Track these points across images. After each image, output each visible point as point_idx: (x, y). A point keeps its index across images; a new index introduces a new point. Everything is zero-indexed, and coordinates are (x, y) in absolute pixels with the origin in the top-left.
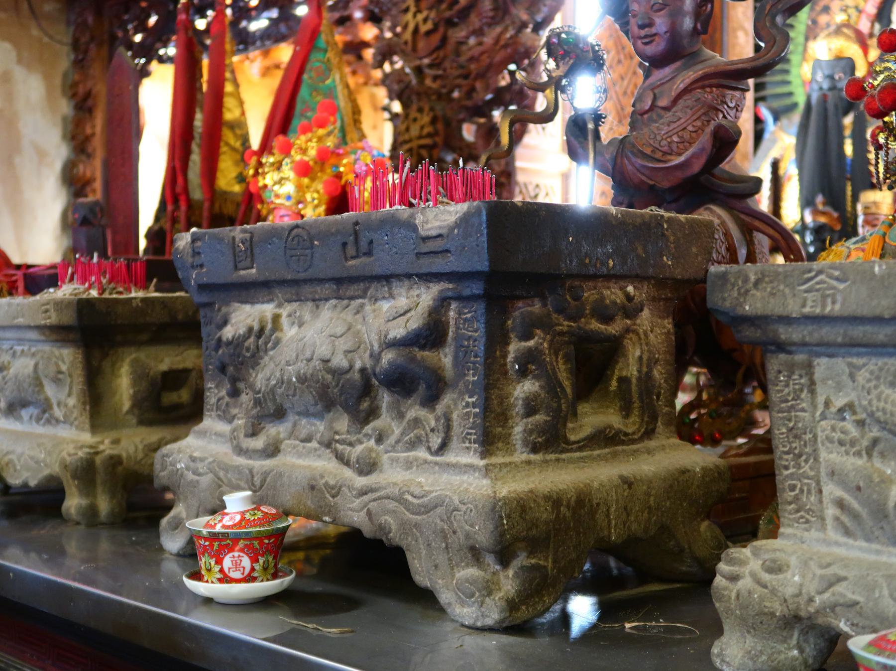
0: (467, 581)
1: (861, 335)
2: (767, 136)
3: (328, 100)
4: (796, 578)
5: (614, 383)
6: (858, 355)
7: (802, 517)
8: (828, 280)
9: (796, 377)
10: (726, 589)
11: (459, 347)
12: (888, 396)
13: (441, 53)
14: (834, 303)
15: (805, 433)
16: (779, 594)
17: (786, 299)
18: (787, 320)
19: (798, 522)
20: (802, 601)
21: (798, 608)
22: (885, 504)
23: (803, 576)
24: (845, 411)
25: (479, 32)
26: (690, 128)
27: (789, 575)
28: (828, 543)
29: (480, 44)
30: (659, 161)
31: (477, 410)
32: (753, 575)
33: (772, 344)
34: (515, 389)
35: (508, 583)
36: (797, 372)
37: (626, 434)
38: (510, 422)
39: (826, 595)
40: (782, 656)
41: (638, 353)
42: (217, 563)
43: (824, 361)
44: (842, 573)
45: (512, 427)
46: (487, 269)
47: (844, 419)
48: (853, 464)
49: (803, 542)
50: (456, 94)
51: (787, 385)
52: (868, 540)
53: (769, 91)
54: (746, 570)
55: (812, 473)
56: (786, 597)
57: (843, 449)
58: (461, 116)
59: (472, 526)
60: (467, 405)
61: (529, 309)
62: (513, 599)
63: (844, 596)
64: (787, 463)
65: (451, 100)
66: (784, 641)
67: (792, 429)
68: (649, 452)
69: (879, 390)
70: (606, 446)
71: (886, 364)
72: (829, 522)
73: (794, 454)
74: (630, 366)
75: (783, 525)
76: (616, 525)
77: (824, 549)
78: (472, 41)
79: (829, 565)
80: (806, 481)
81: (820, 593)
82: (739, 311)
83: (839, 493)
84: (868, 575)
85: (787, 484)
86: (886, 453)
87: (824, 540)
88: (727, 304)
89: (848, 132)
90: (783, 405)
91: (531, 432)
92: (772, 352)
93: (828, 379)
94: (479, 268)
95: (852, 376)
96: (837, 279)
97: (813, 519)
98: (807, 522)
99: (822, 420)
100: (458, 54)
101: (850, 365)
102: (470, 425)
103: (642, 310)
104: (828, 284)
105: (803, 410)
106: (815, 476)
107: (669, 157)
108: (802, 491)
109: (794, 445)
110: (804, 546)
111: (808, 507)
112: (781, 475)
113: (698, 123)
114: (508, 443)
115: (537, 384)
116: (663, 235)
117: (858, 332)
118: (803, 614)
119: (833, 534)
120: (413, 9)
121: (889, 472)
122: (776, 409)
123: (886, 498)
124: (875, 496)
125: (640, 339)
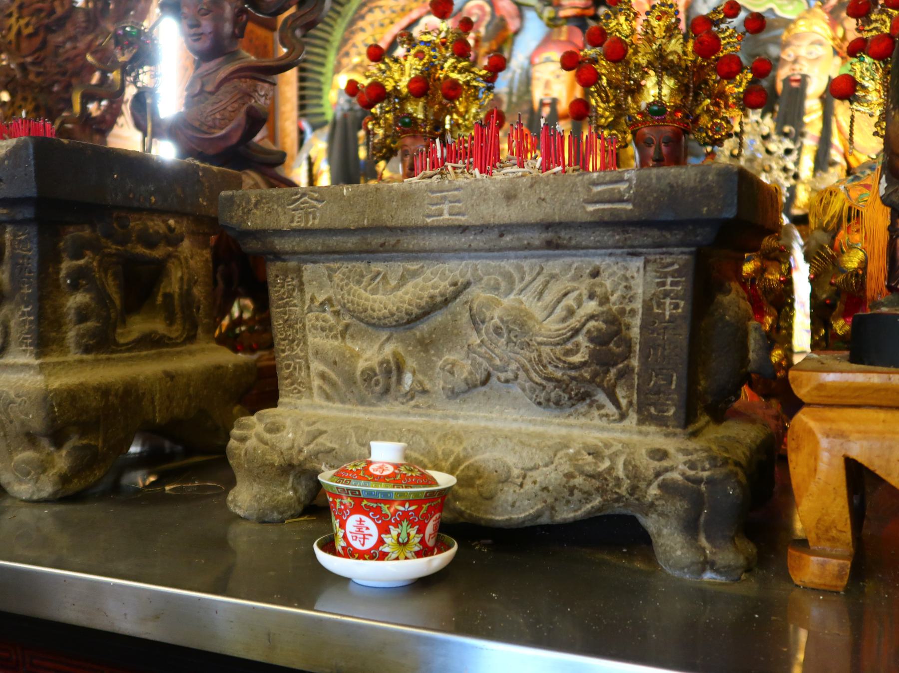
0: (23, 462)
2: (306, 142)
4: (290, 435)
5: (160, 299)
6: (334, 260)
7: (295, 389)
10: (237, 448)
11: (15, 265)
12: (356, 291)
13: (42, 54)
14: (314, 218)
18: (280, 233)
20: (294, 452)
21: (291, 458)
23: (295, 433)
25: (73, 39)
26: (230, 109)
27: (284, 433)
28: (314, 406)
29: (75, 48)
30: (206, 133)
31: (32, 318)
32: (258, 436)
33: (270, 254)
34: (68, 301)
35: (62, 461)
37: (170, 339)
38: (64, 328)
39: (312, 446)
40: (281, 497)
41: (179, 274)
42: (418, 532)
43: (310, 266)
44: (324, 428)
45: (66, 332)
46: (35, 195)
47: (324, 311)
50: (56, 88)
51: (283, 287)
52: (343, 402)
53: (309, 111)
54: (252, 432)
58: (61, 106)
59: (27, 415)
60: (23, 314)
61: (80, 233)
62: (65, 474)
63: (324, 445)
65: (51, 93)
66: (283, 484)
67: (287, 320)
68: (191, 353)
70: (152, 348)
71: (354, 267)
74: (174, 282)
76: (160, 410)
77: (310, 412)
78: (68, 45)
79: (314, 423)
81: (307, 444)
82: (244, 226)
83: (322, 367)
87: (312, 405)
88: (234, 221)
89: (361, 142)
91: (83, 336)
92: (272, 261)
94: (28, 194)
95: (330, 277)
96: (316, 200)
98: (299, 392)
100: (56, 54)
101: (329, 268)
102: (26, 331)
103: (182, 240)
105: (295, 305)
107: (213, 130)
108: (295, 368)
110: (297, 411)
113: (236, 105)
114: (62, 346)
115: (88, 296)
116: (199, 181)
117: (333, 241)
118: (295, 462)
119: (318, 400)
120: (15, 15)
123: (355, 368)
125: (181, 263)
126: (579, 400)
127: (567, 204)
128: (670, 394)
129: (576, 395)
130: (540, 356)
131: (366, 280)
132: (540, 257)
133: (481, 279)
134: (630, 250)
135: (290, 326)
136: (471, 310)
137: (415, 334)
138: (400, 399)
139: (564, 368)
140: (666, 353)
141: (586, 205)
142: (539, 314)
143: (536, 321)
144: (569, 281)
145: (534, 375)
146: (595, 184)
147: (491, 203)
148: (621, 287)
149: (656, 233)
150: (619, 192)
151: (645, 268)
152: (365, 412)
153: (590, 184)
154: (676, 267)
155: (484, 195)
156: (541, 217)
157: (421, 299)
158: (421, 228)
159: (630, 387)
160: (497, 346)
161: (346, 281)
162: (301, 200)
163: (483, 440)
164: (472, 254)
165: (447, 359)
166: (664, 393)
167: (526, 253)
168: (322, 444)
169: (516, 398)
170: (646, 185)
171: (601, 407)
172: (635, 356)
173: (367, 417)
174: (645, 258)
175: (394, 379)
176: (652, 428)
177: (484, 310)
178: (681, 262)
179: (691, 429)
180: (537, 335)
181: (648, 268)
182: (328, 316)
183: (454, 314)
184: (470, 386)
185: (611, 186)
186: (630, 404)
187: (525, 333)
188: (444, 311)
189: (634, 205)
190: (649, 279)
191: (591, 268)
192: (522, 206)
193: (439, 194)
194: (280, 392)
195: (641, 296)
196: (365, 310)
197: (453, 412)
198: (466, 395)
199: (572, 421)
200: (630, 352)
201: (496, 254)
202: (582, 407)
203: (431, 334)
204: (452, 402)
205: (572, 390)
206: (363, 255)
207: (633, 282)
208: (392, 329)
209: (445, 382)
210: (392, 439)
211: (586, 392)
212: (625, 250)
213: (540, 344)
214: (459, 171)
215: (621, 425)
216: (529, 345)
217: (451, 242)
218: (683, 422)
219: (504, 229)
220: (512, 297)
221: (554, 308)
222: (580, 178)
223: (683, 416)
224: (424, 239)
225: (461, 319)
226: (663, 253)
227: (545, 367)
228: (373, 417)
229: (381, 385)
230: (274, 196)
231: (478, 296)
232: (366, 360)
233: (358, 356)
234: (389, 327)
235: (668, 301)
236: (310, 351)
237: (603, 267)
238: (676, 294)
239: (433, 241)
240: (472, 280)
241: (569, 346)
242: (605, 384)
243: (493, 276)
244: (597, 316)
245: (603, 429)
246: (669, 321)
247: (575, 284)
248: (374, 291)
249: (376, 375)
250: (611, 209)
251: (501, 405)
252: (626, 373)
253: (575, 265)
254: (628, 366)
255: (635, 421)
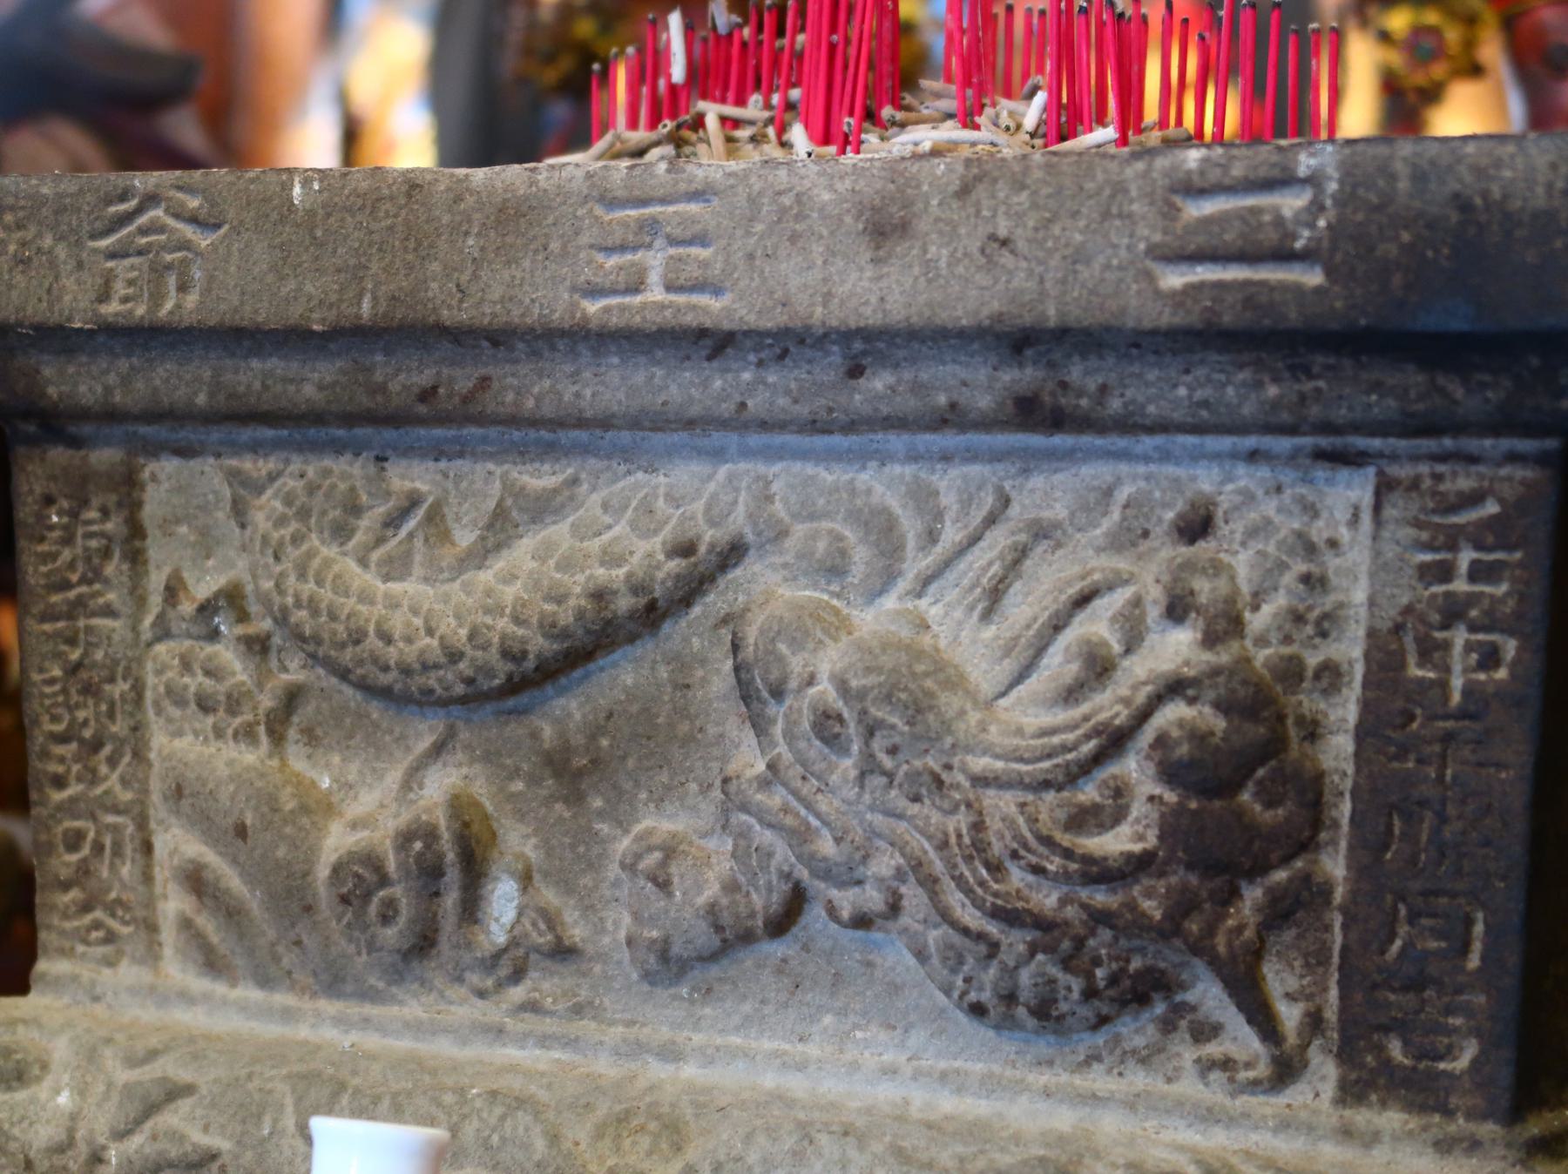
1: (257, 385)
3: (1178, 998)
4: (64, 1099)
6: (255, 448)
7: (97, 925)
8: (171, 222)
9: (93, 514)
12: (327, 563)
14: (183, 288)
15: (112, 680)
16: (13, 1146)
17: (57, 278)
18: (59, 339)
19: (87, 943)
22: (306, 874)
23: (81, 1091)
24: (216, 611)
27: (42, 1091)
28: (156, 994)
33: (27, 415)
36: (96, 502)
39: (137, 1140)
44: (184, 1075)
47: (214, 635)
48: (230, 763)
49: (96, 999)
51: (68, 540)
52: (265, 982)
55: (126, 796)
56: (32, 1154)
57: (210, 720)
63: (180, 1138)
64: (60, 769)
67: (76, 668)
69: (304, 547)
71: (327, 473)
72: (168, 935)
73: (82, 741)
75: (46, 952)
77: (148, 1014)
79: (152, 1055)
80: (111, 819)
81: (120, 1135)
84: (250, 1077)
85: (60, 829)
86: (319, 732)
87: (152, 989)
90: (55, 598)
92: (32, 441)
93: (178, 521)
95: (239, 511)
96: (194, 220)
97: (126, 930)
98: (110, 938)
99: (159, 639)
101: (234, 476)
104: (173, 231)
105: (109, 612)
106: (132, 802)
108: (98, 848)
109: (81, 715)
110: (99, 1009)
111: (113, 895)
112: (44, 802)
117: (253, 376)
119: (177, 971)
121: (326, 783)
122: (35, 610)
124: (281, 852)
126: (1123, 1003)
127: (1088, 262)
128: (1459, 991)
129: (1113, 980)
130: (978, 826)
131: (366, 524)
132: (996, 457)
133: (783, 533)
134: (1324, 442)
135: (89, 690)
136: (736, 648)
137: (535, 735)
138: (474, 978)
139: (1065, 877)
140: (1447, 833)
141: (1157, 268)
142: (984, 673)
143: (972, 695)
144: (1099, 550)
145: (955, 899)
146: (1194, 189)
147: (818, 249)
148: (1288, 579)
149: (1415, 378)
150: (1279, 221)
151: (1377, 508)
152: (340, 1021)
153: (1173, 190)
154: (1491, 508)
155: (793, 217)
156: (996, 306)
157: (560, 600)
158: (563, 333)
159: (1316, 959)
160: (825, 787)
161: (294, 526)
162: (143, 220)
163: (761, 1139)
164: (755, 440)
165: (649, 832)
166: (1439, 983)
167: (948, 440)
168: (177, 1137)
169: (895, 989)
170: (1374, 199)
171: (1205, 1032)
172: (1334, 842)
173: (347, 1040)
174: (1380, 473)
175: (451, 900)
176: (1393, 1119)
177: (782, 648)
178: (1507, 491)
179: (1534, 1128)
180: (968, 749)
181: (1390, 512)
182: (227, 654)
183: (682, 664)
184: (732, 938)
185: (1250, 201)
186: (1314, 1022)
187: (927, 740)
188: (646, 648)
189: (1329, 272)
190: (1390, 551)
191: (1180, 505)
192: (928, 265)
193: (633, 213)
194: (43, 936)
195: (1363, 612)
196: (357, 638)
197: (665, 1033)
198: (714, 971)
199: (1098, 1080)
200: (1316, 824)
201: (837, 440)
202: (1137, 1030)
203: (594, 734)
204: (662, 994)
205: (1097, 962)
206: (361, 432)
207: (1332, 562)
208: (456, 710)
209: (636, 916)
210: (397, 1114)
211: (1148, 971)
212: (1307, 441)
213: (982, 781)
214: (743, 133)
215: (1280, 1100)
216: (939, 783)
217: (674, 393)
218: (1504, 1102)
219: (863, 347)
220: (890, 602)
221: (1040, 651)
222: (1140, 166)
223: (1505, 1075)
224: (574, 377)
225: (704, 681)
226: (1443, 458)
227: (996, 868)
228: (372, 1041)
229: (402, 920)
230: (44, 201)
231: (768, 596)
232: (354, 825)
233: (328, 808)
234: (445, 703)
235: (1460, 637)
236: (156, 787)
237: (1224, 502)
238: (1489, 613)
239: (611, 385)
240: (750, 537)
241: (1089, 793)
242: (1221, 943)
243: (826, 525)
244: (1195, 682)
245: (1209, 1116)
246: (1462, 714)
247: (1122, 564)
248: (395, 568)
249: (384, 881)
250: (1247, 283)
251: (842, 1013)
252: (1299, 904)
253: (1123, 493)
254: (1306, 879)
255: (1329, 1090)
